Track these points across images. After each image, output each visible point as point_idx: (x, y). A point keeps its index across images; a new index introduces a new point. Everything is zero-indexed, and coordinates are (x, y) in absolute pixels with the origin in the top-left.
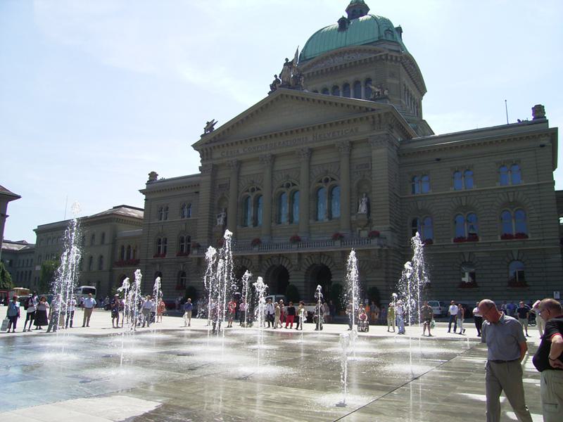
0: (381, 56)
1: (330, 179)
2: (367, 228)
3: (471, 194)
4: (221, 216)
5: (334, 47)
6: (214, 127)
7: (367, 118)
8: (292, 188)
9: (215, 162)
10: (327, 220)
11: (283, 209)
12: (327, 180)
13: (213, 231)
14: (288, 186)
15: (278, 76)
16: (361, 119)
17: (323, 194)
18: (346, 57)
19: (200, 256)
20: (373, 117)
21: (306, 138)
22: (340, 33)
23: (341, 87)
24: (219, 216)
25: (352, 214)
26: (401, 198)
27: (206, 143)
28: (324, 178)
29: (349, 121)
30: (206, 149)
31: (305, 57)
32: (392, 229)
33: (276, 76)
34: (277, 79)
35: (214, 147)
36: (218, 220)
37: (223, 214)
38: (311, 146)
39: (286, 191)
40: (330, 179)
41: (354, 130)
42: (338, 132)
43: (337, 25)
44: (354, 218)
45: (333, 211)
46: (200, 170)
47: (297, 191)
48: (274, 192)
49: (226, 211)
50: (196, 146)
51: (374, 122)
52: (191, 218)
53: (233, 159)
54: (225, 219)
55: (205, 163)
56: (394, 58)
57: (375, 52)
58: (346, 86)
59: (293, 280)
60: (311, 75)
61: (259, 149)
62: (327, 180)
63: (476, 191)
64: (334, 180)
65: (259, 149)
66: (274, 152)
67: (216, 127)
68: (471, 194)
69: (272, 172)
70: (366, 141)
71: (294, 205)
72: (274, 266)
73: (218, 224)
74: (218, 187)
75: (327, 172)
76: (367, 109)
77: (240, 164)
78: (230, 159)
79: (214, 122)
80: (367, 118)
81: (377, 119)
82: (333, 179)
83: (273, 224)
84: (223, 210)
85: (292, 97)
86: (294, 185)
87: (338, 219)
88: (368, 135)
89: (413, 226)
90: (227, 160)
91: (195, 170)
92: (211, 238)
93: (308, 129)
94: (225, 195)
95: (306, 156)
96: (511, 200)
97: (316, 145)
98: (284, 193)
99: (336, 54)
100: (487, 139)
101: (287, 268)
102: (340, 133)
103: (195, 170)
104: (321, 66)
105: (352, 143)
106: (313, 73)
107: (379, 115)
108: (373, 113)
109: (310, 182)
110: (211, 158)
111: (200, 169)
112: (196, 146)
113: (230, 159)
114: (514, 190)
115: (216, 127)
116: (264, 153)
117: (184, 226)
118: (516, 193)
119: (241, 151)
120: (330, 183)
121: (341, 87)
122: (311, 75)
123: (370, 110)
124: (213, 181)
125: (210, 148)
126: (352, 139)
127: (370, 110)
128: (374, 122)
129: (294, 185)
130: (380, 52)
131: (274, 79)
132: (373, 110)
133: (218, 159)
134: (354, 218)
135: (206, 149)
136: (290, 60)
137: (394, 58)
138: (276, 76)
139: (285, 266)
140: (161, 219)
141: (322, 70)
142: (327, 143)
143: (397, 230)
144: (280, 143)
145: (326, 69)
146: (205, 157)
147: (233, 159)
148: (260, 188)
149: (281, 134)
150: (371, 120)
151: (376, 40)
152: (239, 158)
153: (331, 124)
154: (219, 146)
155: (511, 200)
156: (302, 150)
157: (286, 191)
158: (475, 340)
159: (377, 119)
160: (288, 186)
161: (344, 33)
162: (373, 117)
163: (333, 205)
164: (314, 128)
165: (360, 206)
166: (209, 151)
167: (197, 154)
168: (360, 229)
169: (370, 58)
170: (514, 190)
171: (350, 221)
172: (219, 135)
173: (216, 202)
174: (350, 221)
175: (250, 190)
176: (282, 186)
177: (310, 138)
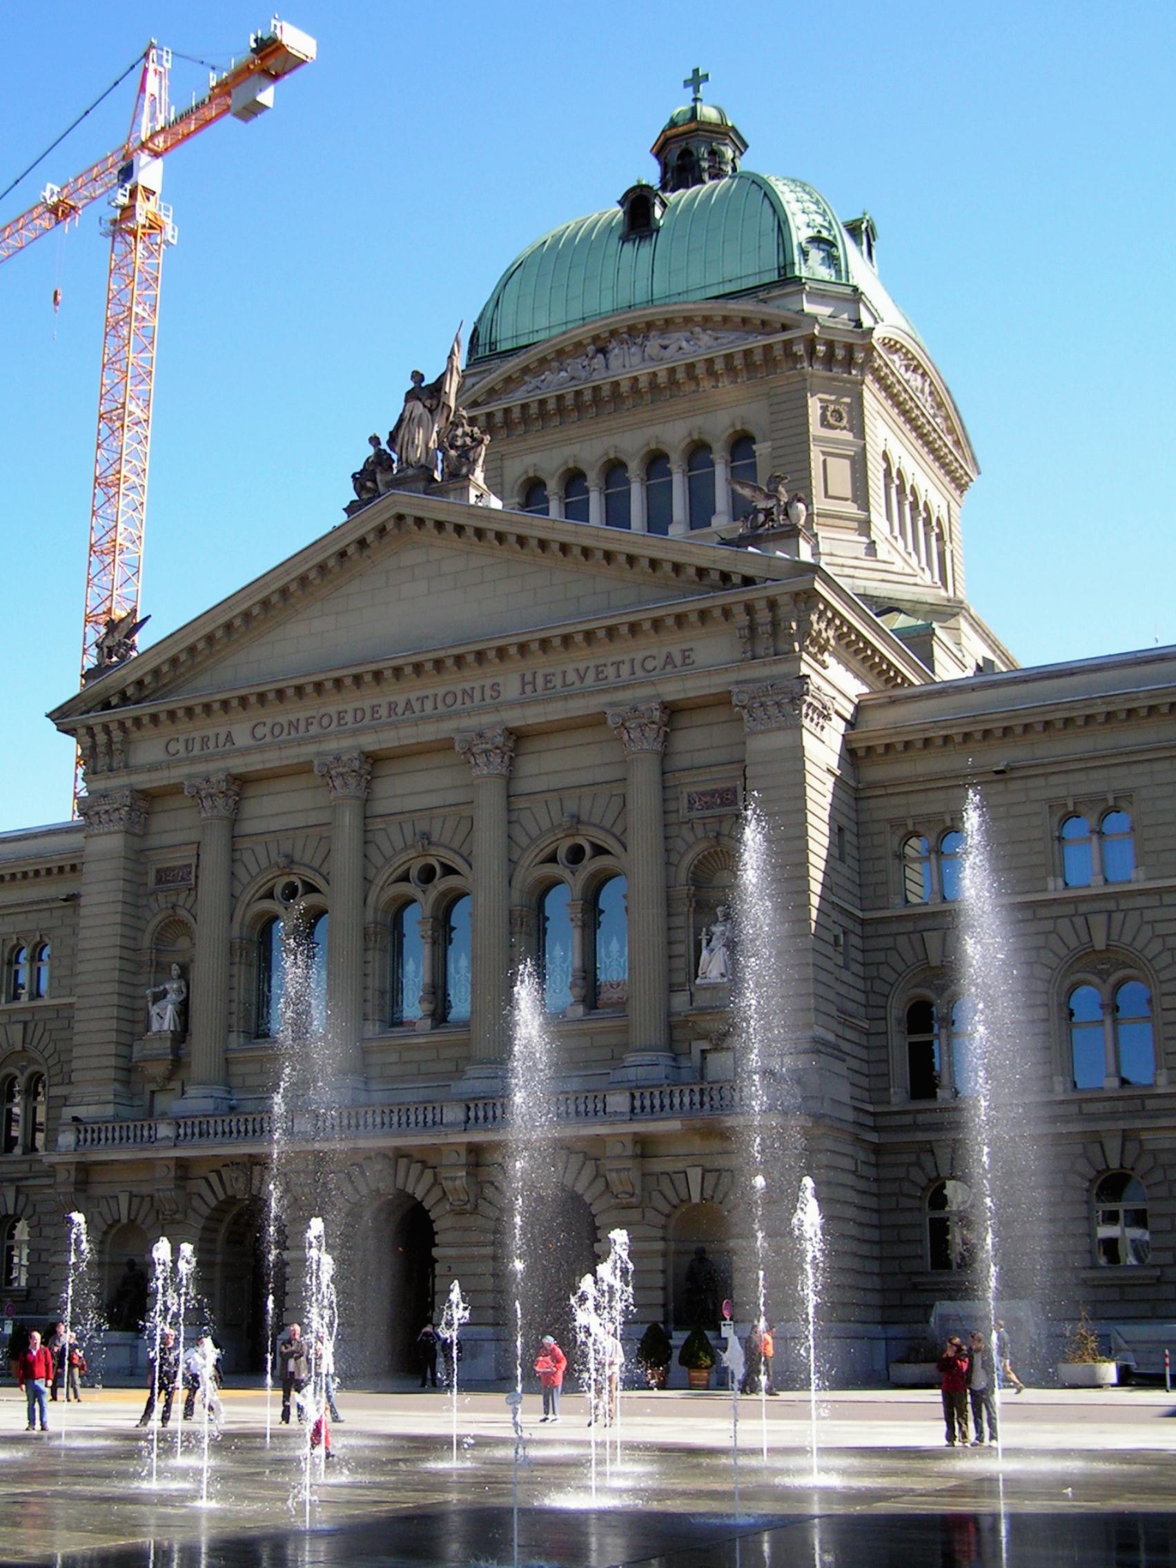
0: (788, 344)
1: (588, 850)
2: (172, 1085)
3: (1124, 904)
4: (164, 994)
5: (607, 306)
6: (137, 638)
7: (727, 613)
8: (442, 884)
9: (143, 781)
10: (580, 1010)
11: (410, 967)
12: (576, 855)
13: (136, 1054)
14: (428, 875)
15: (384, 438)
16: (703, 615)
17: (415, 923)
18: (653, 346)
19: (478, 1137)
20: (749, 609)
21: (494, 686)
22: (628, 247)
23: (553, 487)
24: (159, 997)
25: (672, 988)
26: (863, 922)
27: (107, 706)
28: (568, 842)
29: (657, 624)
30: (106, 729)
31: (492, 344)
32: (826, 1044)
33: (375, 441)
34: (380, 454)
35: (137, 721)
36: (154, 1010)
37: (171, 986)
38: (516, 718)
39: (418, 894)
40: (588, 850)
41: (678, 659)
42: (617, 664)
43: (617, 212)
44: (680, 1001)
45: (451, 992)
46: (83, 813)
47: (458, 895)
48: (371, 900)
49: (184, 974)
50: (63, 717)
51: (752, 628)
52: (46, 1001)
53: (212, 766)
54: (184, 1010)
55: (101, 784)
56: (840, 353)
57: (765, 326)
58: (574, 479)
59: (451, 1252)
60: (516, 414)
61: (314, 730)
62: (576, 855)
63: (1142, 893)
64: (607, 852)
65: (314, 730)
66: (370, 742)
67: (143, 640)
68: (1124, 904)
69: (234, 839)
70: (722, 701)
71: (452, 949)
72: (232, 1200)
73: (155, 1027)
74: (152, 877)
75: (577, 819)
76: (725, 577)
77: (241, 784)
78: (200, 768)
79: (139, 618)
80: (727, 613)
81: (763, 616)
82: (599, 850)
83: (235, 1040)
84: (175, 970)
85: (440, 525)
86: (449, 870)
87: (465, 1025)
88: (734, 677)
89: (912, 1030)
90: (185, 770)
91: (63, 811)
92: (127, 1083)
93: (501, 652)
94: (182, 913)
95: (352, 782)
96: (1100, 943)
97: (532, 716)
98: (412, 901)
99: (613, 333)
100: (974, 719)
101: (426, 1205)
102: (625, 670)
103: (63, 811)
104: (554, 383)
105: (672, 711)
106: (524, 407)
107: (772, 605)
108: (748, 594)
109: (512, 863)
110: (126, 766)
111: (84, 807)
112: (63, 717)
113: (200, 768)
114: (1111, 905)
115: (143, 640)
116: (331, 746)
117: (17, 1032)
118: (1117, 918)
119: (242, 738)
120: (590, 865)
121: (553, 487)
122: (516, 414)
123: (736, 579)
124: (137, 856)
125: (122, 724)
126: (672, 691)
127: (736, 579)
128: (752, 628)
129: (449, 870)
130: (785, 328)
131: (370, 451)
132: (748, 581)
133: (154, 768)
134: (680, 1001)
135: (106, 729)
136: (429, 380)
137: (840, 353)
138: (375, 441)
139: (418, 1196)
140: (17, 997)
141: (560, 398)
142: (578, 707)
143: (846, 1046)
144: (392, 707)
145: (578, 394)
146: (102, 762)
147: (212, 766)
148: (319, 882)
149: (398, 671)
150: (742, 619)
151: (766, 279)
152: (238, 765)
153: (589, 636)
154: (154, 718)
155: (1100, 943)
156: (338, 759)
157: (418, 894)
158: (150, 1405)
159: (763, 616)
160: (428, 875)
161: (646, 250)
162: (749, 609)
163: (601, 952)
164: (523, 648)
165: (705, 953)
166: (117, 735)
167: (69, 747)
168: (705, 1045)
169: (748, 353)
170: (1111, 905)
171: (669, 1014)
172: (156, 672)
173: (146, 941)
174: (669, 1014)
175: (561, 855)
176: (405, 878)
177: (511, 689)
